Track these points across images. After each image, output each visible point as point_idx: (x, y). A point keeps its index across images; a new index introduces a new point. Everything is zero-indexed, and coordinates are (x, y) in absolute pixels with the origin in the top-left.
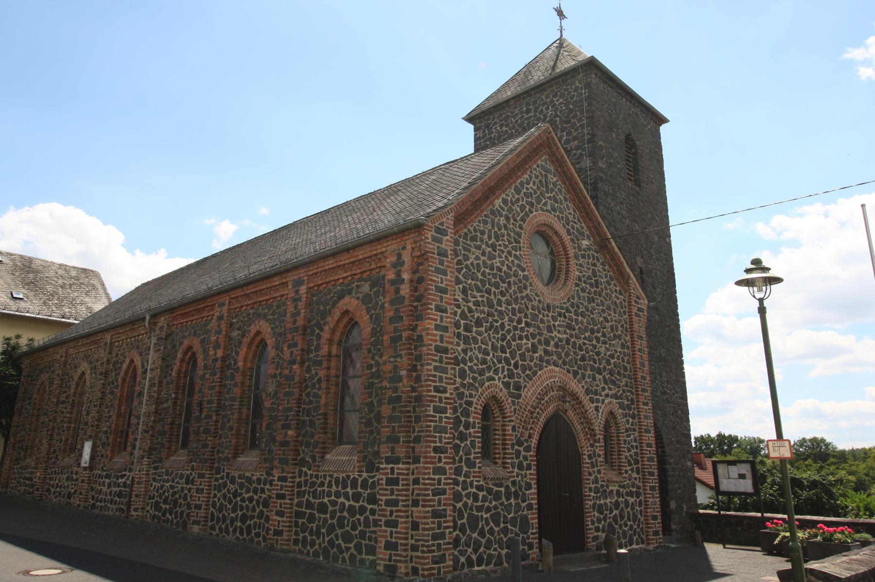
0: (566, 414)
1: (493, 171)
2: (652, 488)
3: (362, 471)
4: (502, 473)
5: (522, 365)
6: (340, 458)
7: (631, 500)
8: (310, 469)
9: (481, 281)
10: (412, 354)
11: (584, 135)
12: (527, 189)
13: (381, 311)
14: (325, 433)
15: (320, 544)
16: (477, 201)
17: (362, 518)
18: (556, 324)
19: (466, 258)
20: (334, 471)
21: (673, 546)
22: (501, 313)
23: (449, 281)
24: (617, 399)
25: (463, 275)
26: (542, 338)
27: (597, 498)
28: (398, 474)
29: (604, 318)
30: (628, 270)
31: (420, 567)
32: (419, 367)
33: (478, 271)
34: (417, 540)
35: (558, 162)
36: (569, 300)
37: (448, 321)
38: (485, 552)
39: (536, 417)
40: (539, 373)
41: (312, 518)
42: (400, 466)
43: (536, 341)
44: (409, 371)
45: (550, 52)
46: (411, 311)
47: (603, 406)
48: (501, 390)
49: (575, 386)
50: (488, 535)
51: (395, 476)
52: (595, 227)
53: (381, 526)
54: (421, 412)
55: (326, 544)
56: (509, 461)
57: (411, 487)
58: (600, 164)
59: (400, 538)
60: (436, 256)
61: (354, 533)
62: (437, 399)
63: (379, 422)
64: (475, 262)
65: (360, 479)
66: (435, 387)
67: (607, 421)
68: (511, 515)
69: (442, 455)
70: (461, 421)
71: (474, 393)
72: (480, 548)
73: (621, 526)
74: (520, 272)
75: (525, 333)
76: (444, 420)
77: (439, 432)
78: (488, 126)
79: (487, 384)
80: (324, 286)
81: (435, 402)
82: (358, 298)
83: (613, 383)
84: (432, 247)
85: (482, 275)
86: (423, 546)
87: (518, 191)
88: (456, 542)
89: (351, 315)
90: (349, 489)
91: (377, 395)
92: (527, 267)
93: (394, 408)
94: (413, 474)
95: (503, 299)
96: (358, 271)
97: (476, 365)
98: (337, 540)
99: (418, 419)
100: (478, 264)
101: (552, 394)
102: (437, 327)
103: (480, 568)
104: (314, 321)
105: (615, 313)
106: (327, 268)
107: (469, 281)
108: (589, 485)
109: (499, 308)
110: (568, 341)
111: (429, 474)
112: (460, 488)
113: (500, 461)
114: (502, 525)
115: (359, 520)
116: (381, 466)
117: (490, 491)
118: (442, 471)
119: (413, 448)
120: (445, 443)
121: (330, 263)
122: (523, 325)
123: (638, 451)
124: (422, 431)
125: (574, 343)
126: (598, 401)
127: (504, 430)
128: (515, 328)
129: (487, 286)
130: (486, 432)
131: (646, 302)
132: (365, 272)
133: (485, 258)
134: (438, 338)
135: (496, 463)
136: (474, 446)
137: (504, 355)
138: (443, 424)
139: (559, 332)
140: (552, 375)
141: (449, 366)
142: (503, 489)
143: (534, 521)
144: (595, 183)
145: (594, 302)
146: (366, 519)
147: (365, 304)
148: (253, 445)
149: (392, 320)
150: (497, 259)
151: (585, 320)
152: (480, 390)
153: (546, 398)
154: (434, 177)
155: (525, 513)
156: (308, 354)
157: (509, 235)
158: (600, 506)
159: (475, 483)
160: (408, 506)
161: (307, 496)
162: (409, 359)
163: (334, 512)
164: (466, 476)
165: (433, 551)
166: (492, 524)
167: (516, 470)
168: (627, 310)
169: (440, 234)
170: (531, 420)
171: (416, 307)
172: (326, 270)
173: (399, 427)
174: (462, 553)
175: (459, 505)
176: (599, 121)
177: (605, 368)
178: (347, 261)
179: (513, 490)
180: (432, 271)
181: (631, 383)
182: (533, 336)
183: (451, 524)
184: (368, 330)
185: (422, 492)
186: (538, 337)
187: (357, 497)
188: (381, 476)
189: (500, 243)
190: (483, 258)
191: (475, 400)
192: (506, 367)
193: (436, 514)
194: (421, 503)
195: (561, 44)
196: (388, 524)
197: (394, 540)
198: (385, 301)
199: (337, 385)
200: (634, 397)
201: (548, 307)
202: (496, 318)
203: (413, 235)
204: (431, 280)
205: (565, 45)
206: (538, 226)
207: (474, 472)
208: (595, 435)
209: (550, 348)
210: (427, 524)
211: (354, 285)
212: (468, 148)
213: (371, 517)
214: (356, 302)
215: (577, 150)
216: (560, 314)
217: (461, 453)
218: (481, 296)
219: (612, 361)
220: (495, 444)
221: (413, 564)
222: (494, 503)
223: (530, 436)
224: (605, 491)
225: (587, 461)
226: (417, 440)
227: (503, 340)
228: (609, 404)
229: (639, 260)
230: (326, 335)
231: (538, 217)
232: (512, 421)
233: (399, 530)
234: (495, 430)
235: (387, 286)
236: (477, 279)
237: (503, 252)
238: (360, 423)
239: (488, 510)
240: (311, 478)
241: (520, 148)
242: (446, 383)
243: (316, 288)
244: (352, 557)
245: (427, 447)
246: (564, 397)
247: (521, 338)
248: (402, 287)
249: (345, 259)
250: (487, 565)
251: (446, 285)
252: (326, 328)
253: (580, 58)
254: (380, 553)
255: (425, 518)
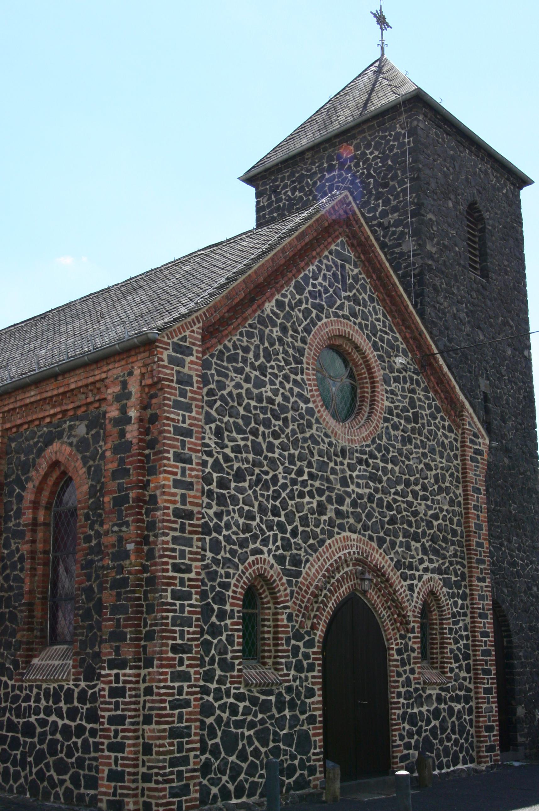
0: (365, 596)
1: (262, 261)
2: (487, 691)
3: (79, 680)
4: (271, 675)
5: (303, 532)
6: (50, 662)
7: (457, 707)
8: (11, 679)
9: (244, 417)
10: (142, 521)
11: (406, 206)
12: (314, 286)
13: (102, 462)
14: (31, 630)
15: (26, 777)
16: (237, 304)
17: (79, 741)
18: (354, 474)
19: (221, 386)
20: (42, 681)
21: (516, 764)
22: (273, 463)
23: (195, 419)
24: (440, 574)
25: (216, 410)
26: (334, 495)
27: (408, 705)
28: (125, 682)
29: (426, 464)
30: (462, 397)
31: (153, 802)
32: (152, 539)
33: (240, 405)
34: (150, 768)
35: (361, 246)
36: (373, 441)
37: (193, 473)
38: (246, 780)
39: (323, 602)
40: (328, 542)
41: (15, 744)
42: (128, 671)
43: (324, 498)
44: (137, 543)
45: (366, 79)
46: (140, 461)
47: (420, 584)
48: (272, 567)
49: (381, 559)
50: (251, 758)
51: (121, 685)
52: (415, 339)
53: (102, 751)
54: (154, 599)
55: (34, 776)
56: (283, 660)
57: (142, 699)
58: (429, 247)
59: (128, 766)
60: (174, 385)
61: (69, 761)
62: (177, 582)
63: (100, 613)
64: (235, 392)
65: (77, 691)
66: (174, 565)
67: (425, 604)
68: (285, 731)
69: (185, 656)
70: (213, 610)
71: (231, 571)
72: (239, 775)
73: (441, 742)
74: (302, 405)
75: (308, 488)
76: (187, 609)
77: (180, 625)
78: (275, 191)
79: (251, 559)
80: (26, 426)
81: (175, 585)
82: (71, 444)
83: (436, 552)
84: (170, 372)
85: (245, 409)
86: (157, 774)
87: (300, 289)
88: (206, 769)
89: (62, 468)
90: (62, 704)
91: (97, 577)
92: (313, 396)
93: (119, 595)
94: (144, 681)
95: (277, 442)
96: (71, 406)
97: (234, 533)
98: (49, 771)
99: (150, 609)
100: (239, 395)
101: (346, 569)
102: (177, 484)
103: (239, 801)
104: (14, 477)
105: (442, 457)
106: (28, 401)
107: (226, 419)
108: (398, 688)
109: (270, 455)
110: (371, 498)
111: (165, 680)
112: (211, 698)
113: (270, 661)
114: (271, 745)
115: (75, 743)
116: (103, 672)
117: (254, 701)
118: (185, 677)
119: (145, 647)
120: (189, 640)
121: (32, 395)
122: (305, 477)
123: (470, 642)
124: (156, 625)
125: (381, 499)
126: (413, 577)
127: (277, 620)
128: (294, 482)
129: (253, 424)
130: (250, 625)
131: (487, 441)
132: (79, 407)
133: (250, 386)
134: (178, 498)
135: (264, 664)
136: (231, 643)
137: (276, 519)
138: (186, 614)
139: (358, 485)
140: (347, 544)
141: (195, 537)
142: (273, 698)
143: (317, 738)
144: (420, 276)
145: (410, 442)
146: (85, 742)
147: (81, 452)
148: (55, 639)
149: (116, 475)
150: (268, 386)
151: (397, 469)
152: (241, 567)
153: (338, 576)
154: (187, 268)
155: (305, 728)
156: (6, 523)
157: (286, 352)
158: (413, 715)
159: (233, 691)
160: (138, 723)
161: (8, 715)
162: (139, 528)
163: (44, 734)
164: (221, 681)
165: (172, 781)
166: (257, 743)
167: (293, 672)
168: (459, 453)
169: (181, 353)
170: (316, 606)
171: (147, 456)
172: (27, 405)
173: (126, 619)
174: (214, 782)
175: (210, 720)
176: (428, 184)
177: (424, 533)
178: (55, 392)
179: (288, 698)
180: (169, 406)
181: (462, 552)
182: (320, 492)
183: (198, 745)
184: (85, 488)
185: (157, 705)
186: (327, 493)
187: (73, 714)
188: (104, 686)
189: (273, 363)
190: (246, 386)
191: (233, 581)
192: (280, 535)
193: (175, 733)
194: (155, 719)
195: (380, 67)
196: (112, 748)
197: (119, 769)
198: (106, 447)
199: (46, 564)
200: (466, 570)
201: (343, 451)
202: (266, 468)
203: (143, 355)
204: (168, 418)
205: (385, 69)
206: (329, 338)
207: (232, 677)
208: (408, 623)
209: (344, 508)
210: (163, 746)
211: (66, 426)
212: (249, 221)
213: (91, 740)
214: (68, 449)
215: (396, 227)
216: (360, 461)
217: (213, 652)
218: (243, 439)
219: (435, 523)
220: (264, 639)
221: (145, 799)
222: (260, 716)
223: (314, 627)
224: (420, 696)
225: (396, 657)
226: (150, 636)
227: (275, 499)
228: (428, 580)
229: (483, 384)
230: (29, 496)
231: (328, 326)
232: (287, 607)
233: (125, 755)
234: (264, 620)
235: (109, 427)
236: (237, 416)
237: (276, 376)
238: (76, 615)
239: (252, 725)
240: (13, 690)
241: (303, 228)
242: (190, 559)
243: (14, 430)
244: (68, 792)
245: (163, 645)
246: (363, 573)
247: (301, 495)
248: (129, 428)
249: (52, 390)
250: (249, 796)
251: (190, 425)
252: (30, 485)
253: (403, 91)
254: (103, 786)
255: (159, 738)
